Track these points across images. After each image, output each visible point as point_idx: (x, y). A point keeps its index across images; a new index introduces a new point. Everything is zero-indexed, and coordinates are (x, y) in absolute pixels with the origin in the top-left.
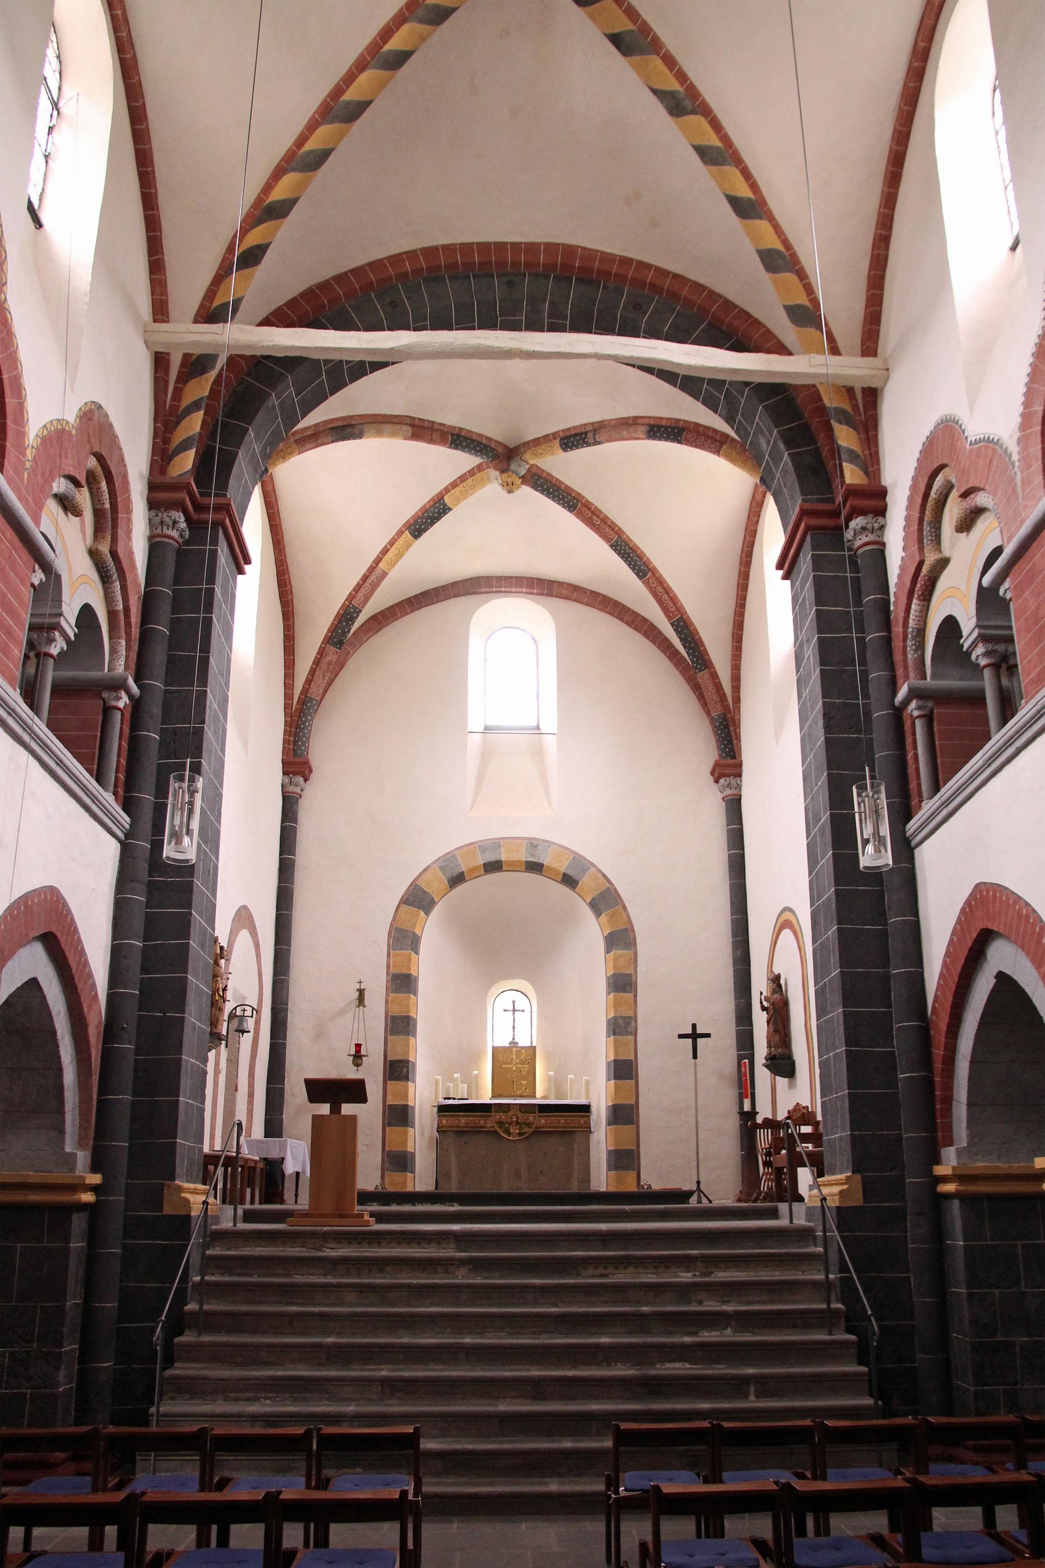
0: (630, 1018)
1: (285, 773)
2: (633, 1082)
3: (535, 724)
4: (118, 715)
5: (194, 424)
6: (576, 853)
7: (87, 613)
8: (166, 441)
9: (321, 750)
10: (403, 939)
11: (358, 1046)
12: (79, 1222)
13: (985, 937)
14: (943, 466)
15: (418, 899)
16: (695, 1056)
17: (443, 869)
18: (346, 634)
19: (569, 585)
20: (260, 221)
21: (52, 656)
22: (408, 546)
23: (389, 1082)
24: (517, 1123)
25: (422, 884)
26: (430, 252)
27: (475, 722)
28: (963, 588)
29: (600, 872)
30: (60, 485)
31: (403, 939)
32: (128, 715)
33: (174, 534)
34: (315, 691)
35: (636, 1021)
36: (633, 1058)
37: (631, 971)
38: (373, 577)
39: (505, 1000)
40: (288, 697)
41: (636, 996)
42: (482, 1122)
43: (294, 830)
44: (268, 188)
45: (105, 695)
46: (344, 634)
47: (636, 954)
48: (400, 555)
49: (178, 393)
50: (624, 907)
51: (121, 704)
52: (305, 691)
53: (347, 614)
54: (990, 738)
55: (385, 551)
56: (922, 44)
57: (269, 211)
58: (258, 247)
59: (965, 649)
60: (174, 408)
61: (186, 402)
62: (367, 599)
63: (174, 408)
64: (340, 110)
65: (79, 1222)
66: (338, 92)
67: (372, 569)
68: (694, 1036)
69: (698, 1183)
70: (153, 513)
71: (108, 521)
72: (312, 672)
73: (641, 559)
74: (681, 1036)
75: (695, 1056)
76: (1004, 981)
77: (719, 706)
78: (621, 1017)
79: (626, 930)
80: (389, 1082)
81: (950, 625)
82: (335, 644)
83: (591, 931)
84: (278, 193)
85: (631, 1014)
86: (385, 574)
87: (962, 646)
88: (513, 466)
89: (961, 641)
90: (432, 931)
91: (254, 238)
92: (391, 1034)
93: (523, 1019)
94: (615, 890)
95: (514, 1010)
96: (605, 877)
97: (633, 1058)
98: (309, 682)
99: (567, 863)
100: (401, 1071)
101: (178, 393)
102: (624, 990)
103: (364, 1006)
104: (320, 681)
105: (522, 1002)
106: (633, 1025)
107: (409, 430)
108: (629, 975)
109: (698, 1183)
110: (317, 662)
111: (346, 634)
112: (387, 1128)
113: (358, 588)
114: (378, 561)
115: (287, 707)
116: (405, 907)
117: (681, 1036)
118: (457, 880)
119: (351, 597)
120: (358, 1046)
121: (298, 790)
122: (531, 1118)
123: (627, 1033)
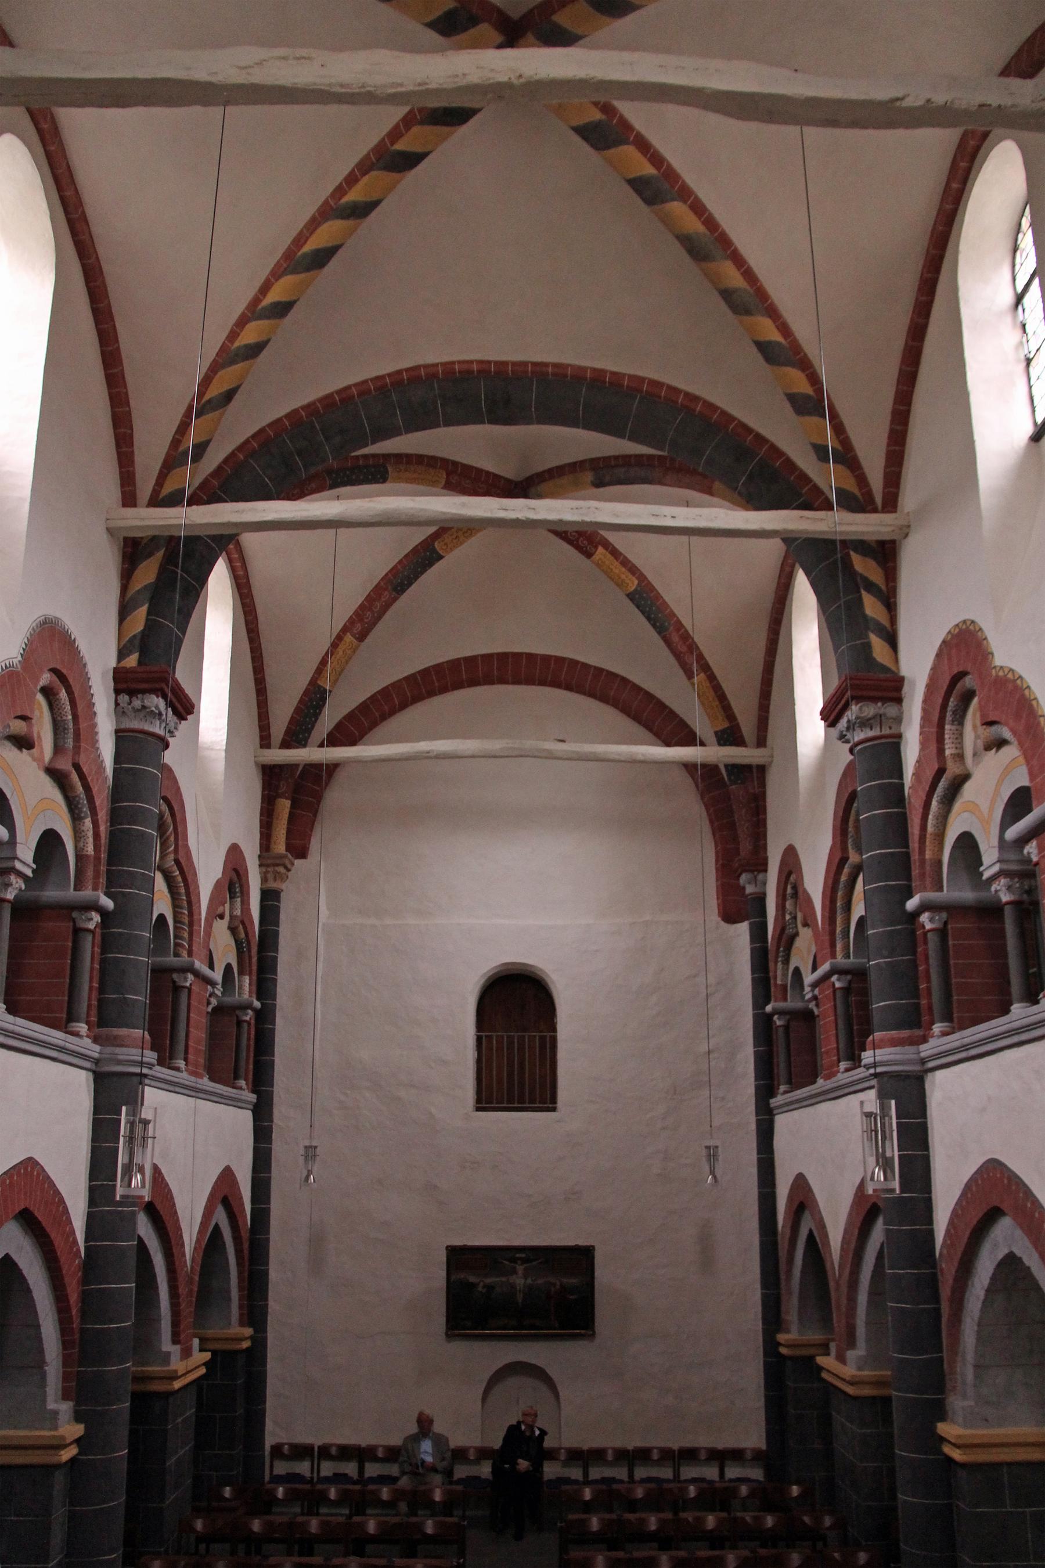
4: (90, 938)
7: (49, 840)
12: (60, 1479)
13: (993, 1215)
14: (962, 674)
20: (233, 362)
28: (985, 807)
32: (98, 938)
45: (75, 914)
51: (91, 926)
54: (1030, 810)
56: (955, 186)
57: (236, 354)
59: (984, 877)
64: (306, 260)
65: (60, 1479)
66: (300, 240)
70: (124, 698)
71: (72, 729)
76: (1011, 1264)
81: (967, 843)
87: (981, 874)
89: (981, 869)
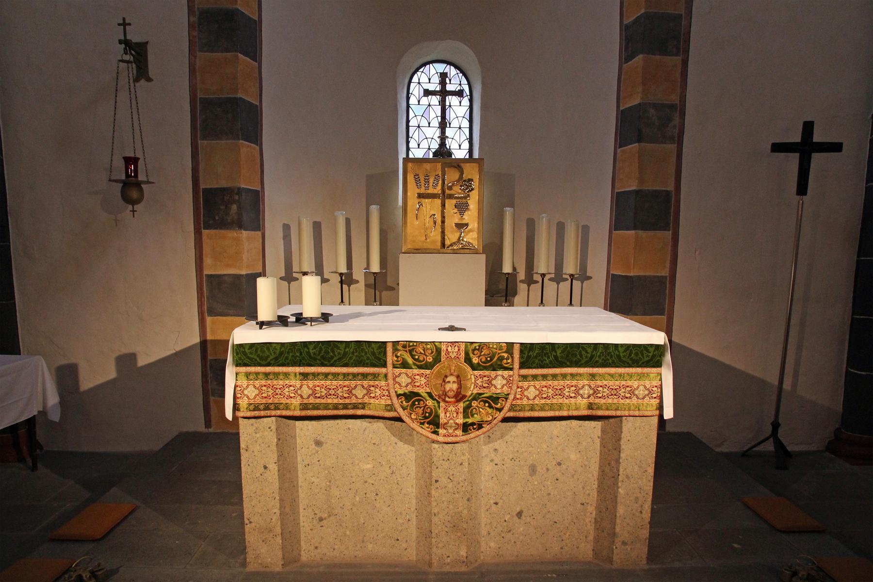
0: (672, 107)
2: (668, 234)
16: (802, 189)
21: (462, 173)
23: (205, 232)
24: (459, 397)
35: (683, 114)
39: (428, 77)
41: (685, 63)
42: (359, 392)
68: (806, 147)
69: (776, 426)
74: (777, 148)
75: (802, 189)
77: (434, 132)
78: (655, 106)
80: (205, 232)
85: (674, 99)
92: (204, 138)
93: (458, 109)
97: (671, 188)
100: (228, 209)
102: (663, 51)
103: (149, 80)
105: (456, 81)
106: (676, 121)
108: (677, 18)
109: (776, 426)
112: (209, 320)
117: (777, 148)
122: (499, 382)
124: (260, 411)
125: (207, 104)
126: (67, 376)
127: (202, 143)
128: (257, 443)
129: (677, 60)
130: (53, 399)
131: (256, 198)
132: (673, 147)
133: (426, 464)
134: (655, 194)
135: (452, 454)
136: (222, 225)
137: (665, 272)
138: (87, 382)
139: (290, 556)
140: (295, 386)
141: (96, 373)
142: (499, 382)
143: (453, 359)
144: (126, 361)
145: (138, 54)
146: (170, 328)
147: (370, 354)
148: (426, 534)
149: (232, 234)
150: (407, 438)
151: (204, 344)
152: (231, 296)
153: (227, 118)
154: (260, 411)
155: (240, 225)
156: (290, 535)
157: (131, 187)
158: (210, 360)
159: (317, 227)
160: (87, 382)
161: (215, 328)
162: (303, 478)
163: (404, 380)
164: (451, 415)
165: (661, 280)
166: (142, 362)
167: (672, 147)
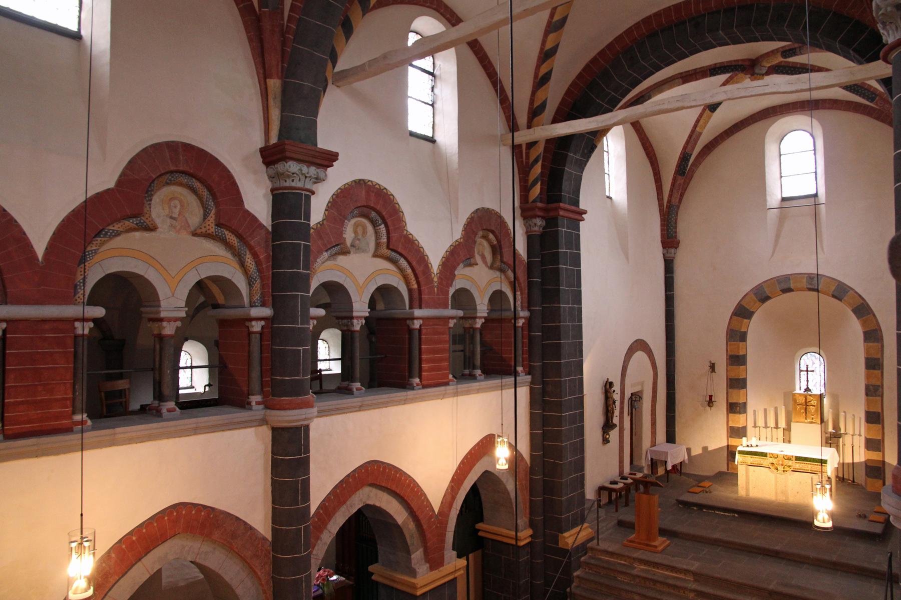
1: (664, 247)
3: (814, 192)
5: (537, 169)
6: (840, 282)
8: (526, 181)
9: (689, 224)
10: (736, 336)
11: (711, 397)
15: (742, 312)
17: (755, 294)
18: (685, 169)
19: (830, 100)
22: (710, 117)
25: (743, 303)
26: (647, 20)
27: (774, 198)
29: (856, 292)
30: (481, 233)
31: (736, 336)
33: (536, 229)
34: (675, 201)
36: (880, 411)
37: (879, 356)
38: (694, 136)
40: (661, 205)
41: (882, 373)
43: (672, 278)
44: (544, 43)
46: (685, 168)
47: (882, 346)
48: (706, 123)
49: (527, 154)
50: (874, 315)
52: (669, 201)
53: (684, 157)
55: (698, 121)
57: (546, 55)
58: (546, 74)
60: (527, 163)
61: (532, 159)
62: (693, 148)
63: (527, 163)
67: (693, 131)
72: (671, 190)
73: (869, 91)
79: (875, 330)
82: (680, 175)
83: (855, 328)
84: (548, 46)
85: (879, 383)
86: (700, 134)
88: (757, 71)
90: (755, 327)
91: (543, 70)
94: (868, 305)
95: (807, 371)
96: (860, 296)
98: (670, 196)
99: (833, 288)
101: (527, 154)
102: (874, 369)
104: (676, 196)
107: (680, 80)
110: (673, 184)
111: (685, 169)
113: (687, 142)
114: (695, 126)
115: (661, 211)
116: (735, 318)
118: (764, 299)
119: (685, 148)
120: (711, 397)
121: (672, 255)
123: (876, 396)
124: (743, 463)
125: (731, 379)
126: (689, 450)
127: (730, 390)
128: (741, 471)
129: (879, 372)
130: (686, 457)
131: (745, 404)
132: (879, 398)
133: (776, 478)
134: (875, 413)
135: (782, 477)
136: (735, 412)
137: (880, 438)
138: (694, 453)
139: (747, 495)
140: (749, 459)
141: (697, 451)
142: (790, 463)
143: (781, 457)
144: (705, 449)
145: (712, 367)
146: (717, 439)
147: (764, 455)
148: (776, 493)
149: (737, 415)
150: (772, 472)
151: (728, 446)
152: (738, 432)
153: (737, 383)
154: (743, 463)
155: (740, 413)
156: (747, 490)
157: (710, 402)
158: (731, 453)
159: (765, 410)
160: (694, 453)
161: (733, 442)
162: (751, 478)
163: (771, 460)
164: (780, 468)
165: (879, 441)
166: (710, 449)
167: (879, 398)
